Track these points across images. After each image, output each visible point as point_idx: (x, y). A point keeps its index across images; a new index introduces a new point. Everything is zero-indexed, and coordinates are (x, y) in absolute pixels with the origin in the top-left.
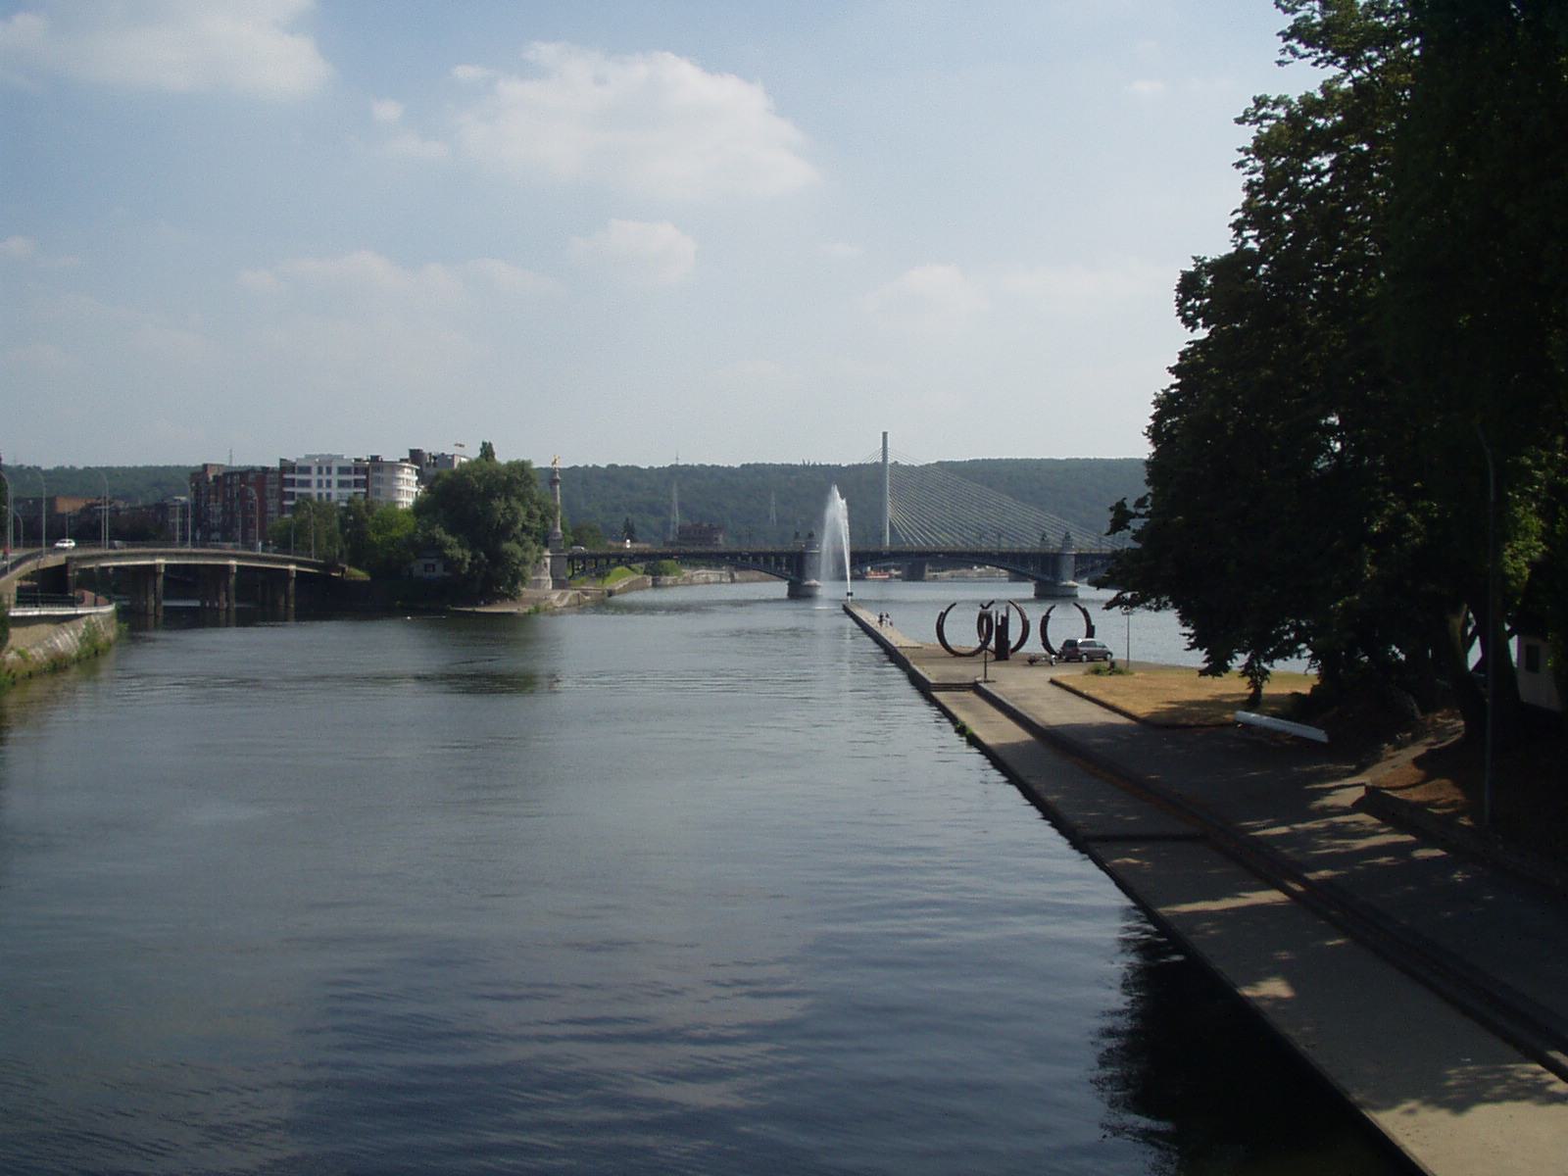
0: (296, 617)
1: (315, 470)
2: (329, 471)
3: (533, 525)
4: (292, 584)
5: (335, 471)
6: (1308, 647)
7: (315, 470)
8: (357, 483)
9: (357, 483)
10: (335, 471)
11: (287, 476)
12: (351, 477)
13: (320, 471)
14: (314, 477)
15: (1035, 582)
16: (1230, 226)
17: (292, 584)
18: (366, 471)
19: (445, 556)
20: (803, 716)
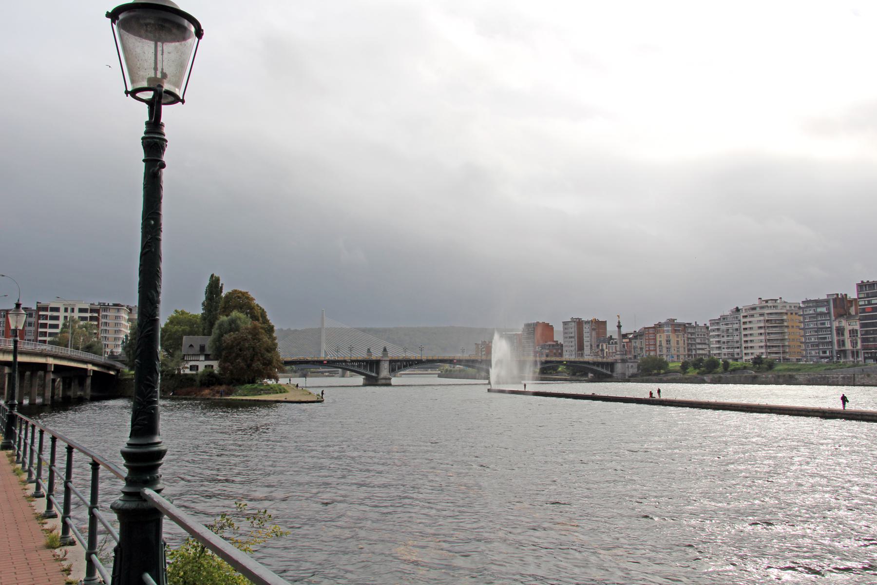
0: (543, 368)
1: (62, 310)
2: (73, 310)
3: (644, 352)
4: (89, 381)
5: (76, 310)
6: (126, 479)
7: (62, 310)
8: (92, 318)
9: (92, 318)
10: (76, 310)
11: (41, 313)
12: (88, 315)
13: (66, 310)
14: (62, 314)
15: (363, 377)
16: (843, 395)
17: (89, 381)
18: (97, 311)
19: (229, 362)
20: (313, 457)
